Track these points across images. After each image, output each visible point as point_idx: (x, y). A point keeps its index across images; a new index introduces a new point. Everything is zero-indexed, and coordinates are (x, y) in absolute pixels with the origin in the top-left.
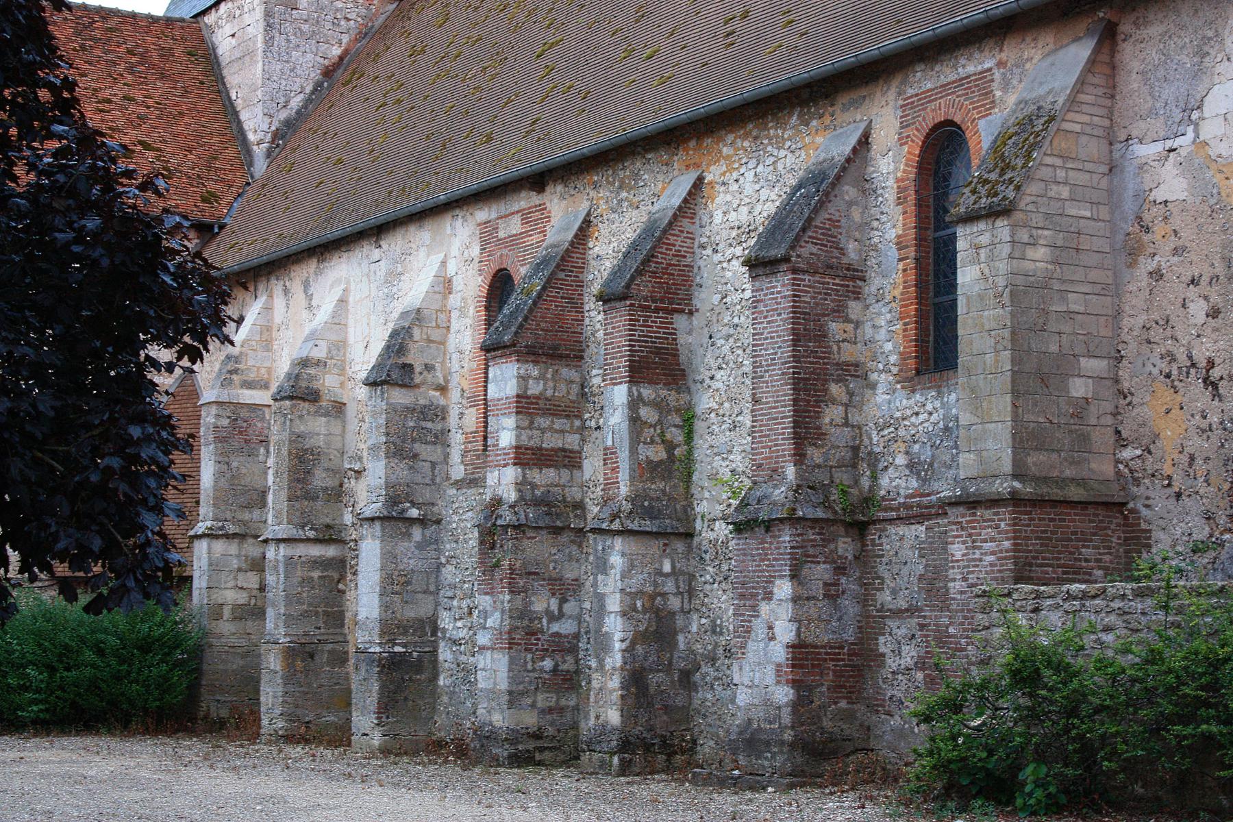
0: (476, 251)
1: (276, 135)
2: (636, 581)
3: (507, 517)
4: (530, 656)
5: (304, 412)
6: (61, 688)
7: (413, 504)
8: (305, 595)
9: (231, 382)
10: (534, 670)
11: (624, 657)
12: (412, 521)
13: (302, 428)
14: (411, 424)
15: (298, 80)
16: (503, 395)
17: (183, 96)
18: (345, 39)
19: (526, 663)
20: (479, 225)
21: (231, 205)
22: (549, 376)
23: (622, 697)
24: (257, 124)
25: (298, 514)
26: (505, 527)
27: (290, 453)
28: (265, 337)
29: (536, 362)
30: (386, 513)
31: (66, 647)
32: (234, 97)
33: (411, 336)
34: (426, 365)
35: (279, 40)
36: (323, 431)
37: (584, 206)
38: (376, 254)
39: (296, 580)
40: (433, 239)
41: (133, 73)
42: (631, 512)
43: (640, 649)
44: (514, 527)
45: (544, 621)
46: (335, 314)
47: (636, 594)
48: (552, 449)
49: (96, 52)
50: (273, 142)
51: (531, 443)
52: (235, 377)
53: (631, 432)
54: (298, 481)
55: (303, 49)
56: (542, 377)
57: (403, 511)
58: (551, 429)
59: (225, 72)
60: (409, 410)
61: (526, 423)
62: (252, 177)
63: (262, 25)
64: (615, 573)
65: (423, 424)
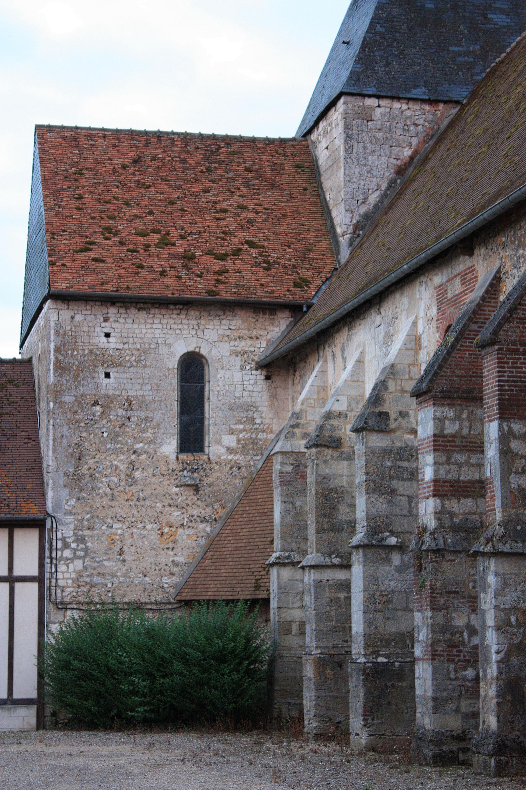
0: (434, 311)
1: (357, 227)
2: (510, 598)
3: (428, 542)
4: (452, 666)
5: (328, 457)
6: (161, 693)
7: (392, 533)
8: (333, 613)
9: (293, 435)
10: (456, 679)
11: (499, 668)
12: (392, 548)
13: (327, 471)
14: (389, 464)
15: (375, 180)
16: (426, 436)
17: (288, 201)
18: (415, 141)
19: (449, 672)
20: (436, 288)
21: (319, 288)
22: (464, 416)
23: (498, 704)
24: (342, 220)
25: (325, 544)
26: (427, 551)
27: (317, 493)
28: (321, 396)
29: (451, 405)
30: (366, 542)
31: (162, 658)
32: (328, 199)
33: (386, 388)
34: (401, 413)
35: (358, 148)
36: (346, 472)
37: (497, 264)
38: (378, 319)
39: (324, 601)
40: (410, 303)
41: (248, 186)
42: (503, 536)
43: (515, 660)
44: (434, 551)
45: (466, 635)
46: (353, 373)
47: (510, 609)
48: (469, 481)
49: (220, 172)
50: (354, 233)
51: (449, 477)
52: (296, 430)
53: (502, 464)
54: (325, 515)
55: (377, 153)
56: (458, 418)
57: (383, 539)
58: (467, 463)
59: (323, 179)
60: (385, 452)
61: (444, 459)
62: (339, 263)
63: (343, 136)
64: (491, 591)
65: (400, 463)
